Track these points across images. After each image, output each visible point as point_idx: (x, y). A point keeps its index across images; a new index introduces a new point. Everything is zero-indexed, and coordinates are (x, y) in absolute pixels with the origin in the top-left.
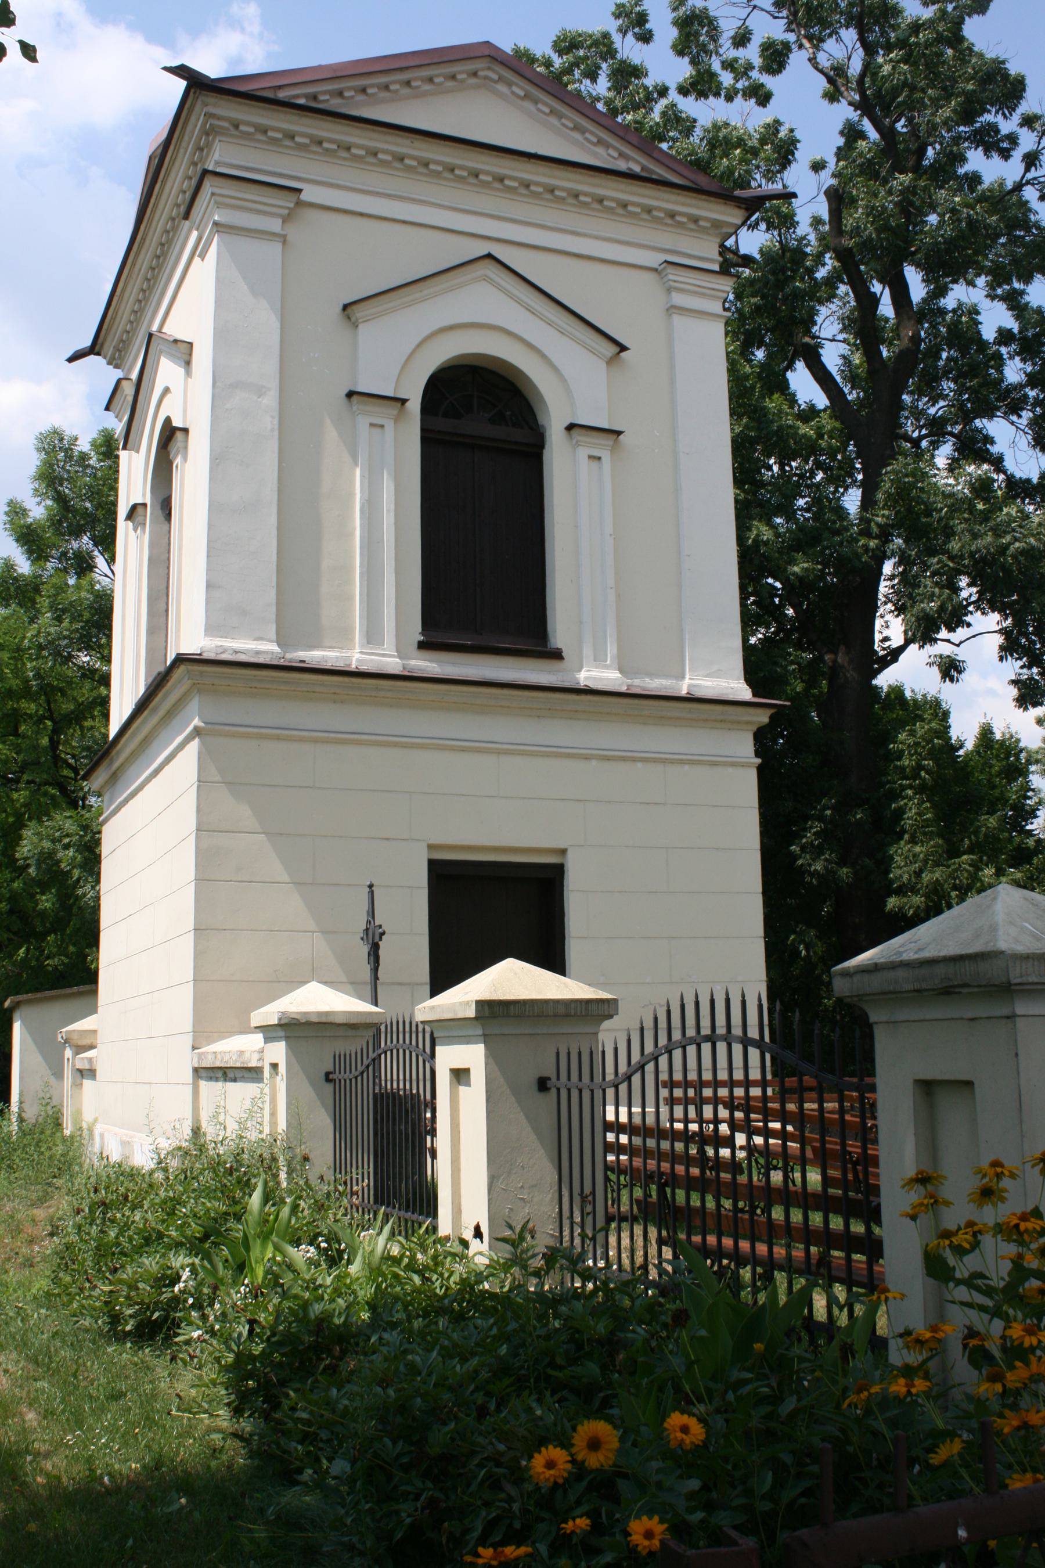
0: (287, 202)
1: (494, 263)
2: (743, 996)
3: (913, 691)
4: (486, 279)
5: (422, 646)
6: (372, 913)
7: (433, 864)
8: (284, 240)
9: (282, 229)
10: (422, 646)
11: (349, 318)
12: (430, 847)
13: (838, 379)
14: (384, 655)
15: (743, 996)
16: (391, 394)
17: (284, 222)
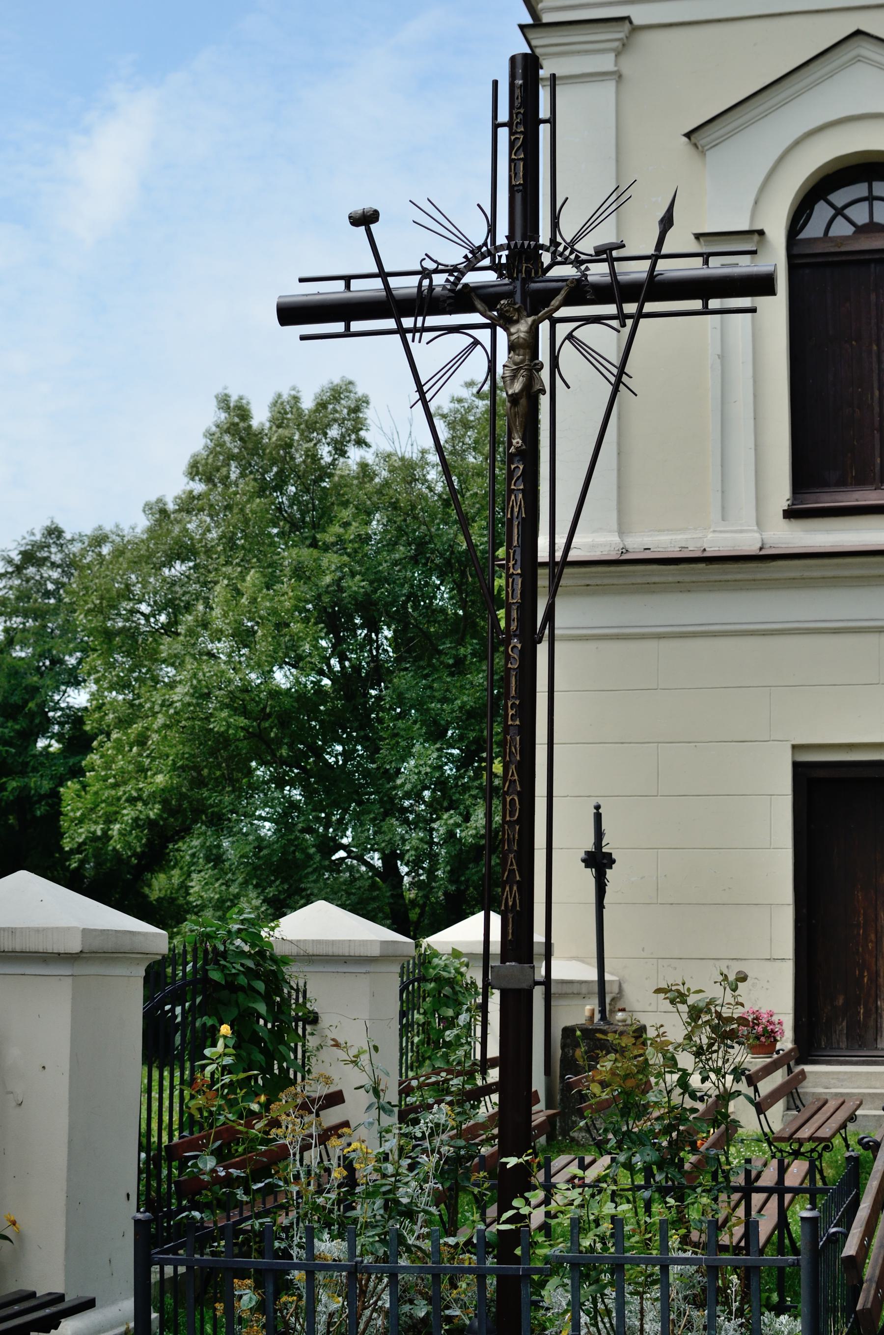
0: (619, 33)
1: (866, 38)
2: (598, 818)
3: (678, 997)
4: (858, 59)
5: (790, 514)
6: (599, 834)
7: (798, 768)
8: (618, 76)
9: (616, 64)
10: (790, 514)
11: (696, 146)
12: (794, 747)
13: (769, 1060)
14: (741, 531)
15: (598, 818)
16: (745, 227)
17: (618, 54)
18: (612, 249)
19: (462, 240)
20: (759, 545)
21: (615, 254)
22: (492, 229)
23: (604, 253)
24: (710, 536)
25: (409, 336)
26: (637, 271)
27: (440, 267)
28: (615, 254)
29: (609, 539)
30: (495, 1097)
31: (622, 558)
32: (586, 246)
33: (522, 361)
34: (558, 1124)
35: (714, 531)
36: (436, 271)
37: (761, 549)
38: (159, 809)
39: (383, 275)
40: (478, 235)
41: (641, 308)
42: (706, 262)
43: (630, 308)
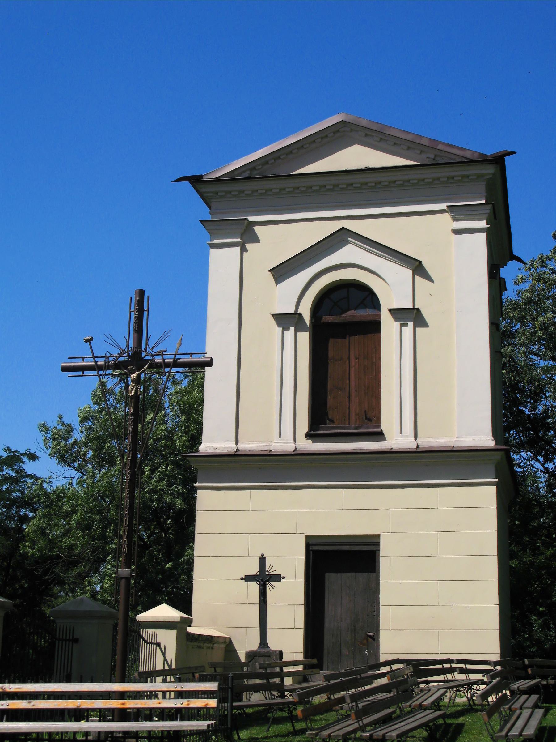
18: (163, 352)
19: (119, 347)
20: (294, 449)
21: (164, 353)
22: (128, 345)
23: (161, 353)
24: (274, 444)
25: (101, 377)
26: (169, 360)
27: (112, 356)
28: (164, 353)
29: (231, 445)
30: (244, 709)
31: (453, 449)
32: (157, 350)
33: (134, 386)
34: (546, 736)
35: (276, 442)
36: (110, 357)
37: (294, 451)
38: (33, 555)
39: (94, 357)
40: (123, 345)
41: (171, 370)
42: (84, 361)
43: (101, 372)
